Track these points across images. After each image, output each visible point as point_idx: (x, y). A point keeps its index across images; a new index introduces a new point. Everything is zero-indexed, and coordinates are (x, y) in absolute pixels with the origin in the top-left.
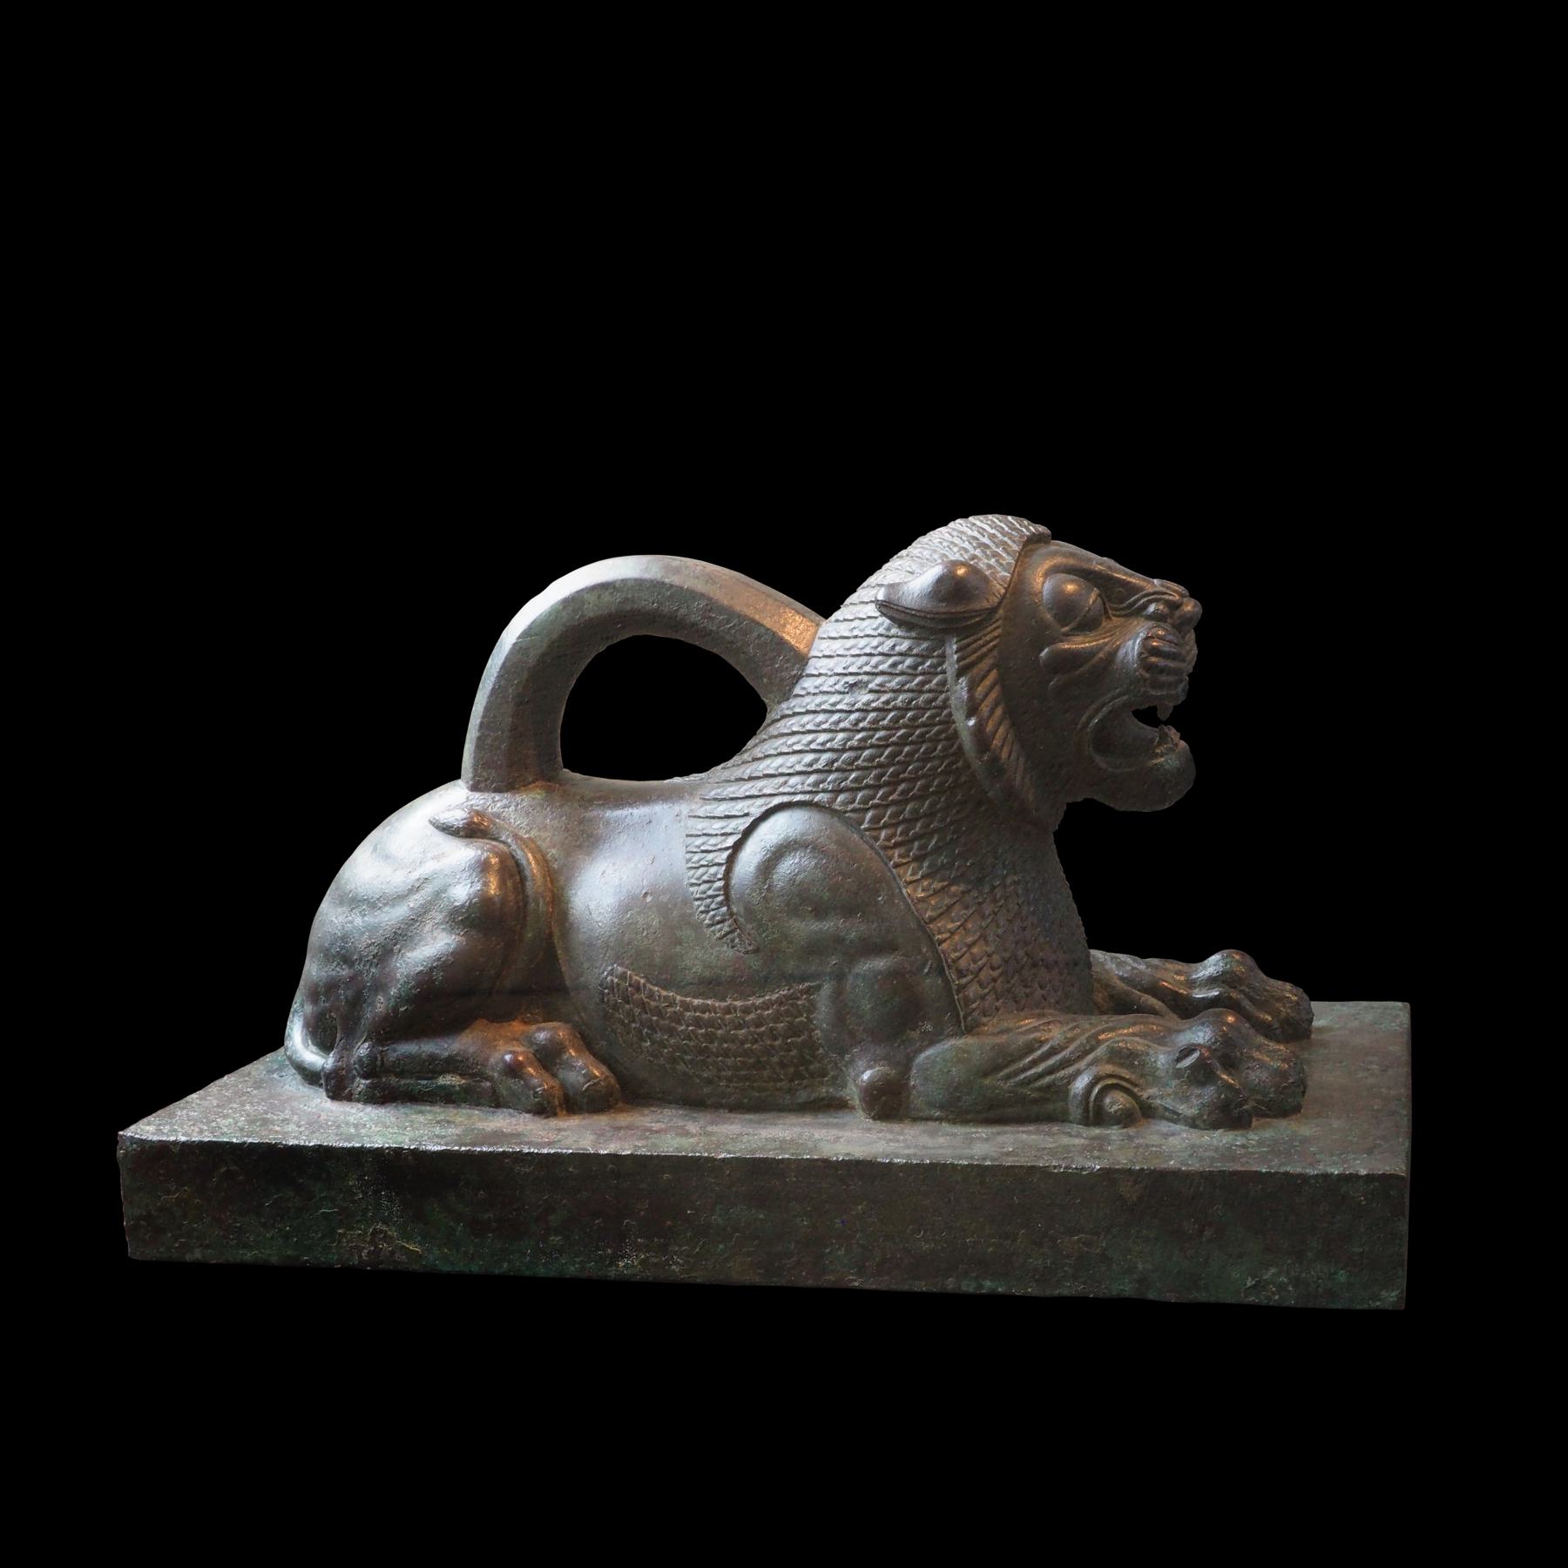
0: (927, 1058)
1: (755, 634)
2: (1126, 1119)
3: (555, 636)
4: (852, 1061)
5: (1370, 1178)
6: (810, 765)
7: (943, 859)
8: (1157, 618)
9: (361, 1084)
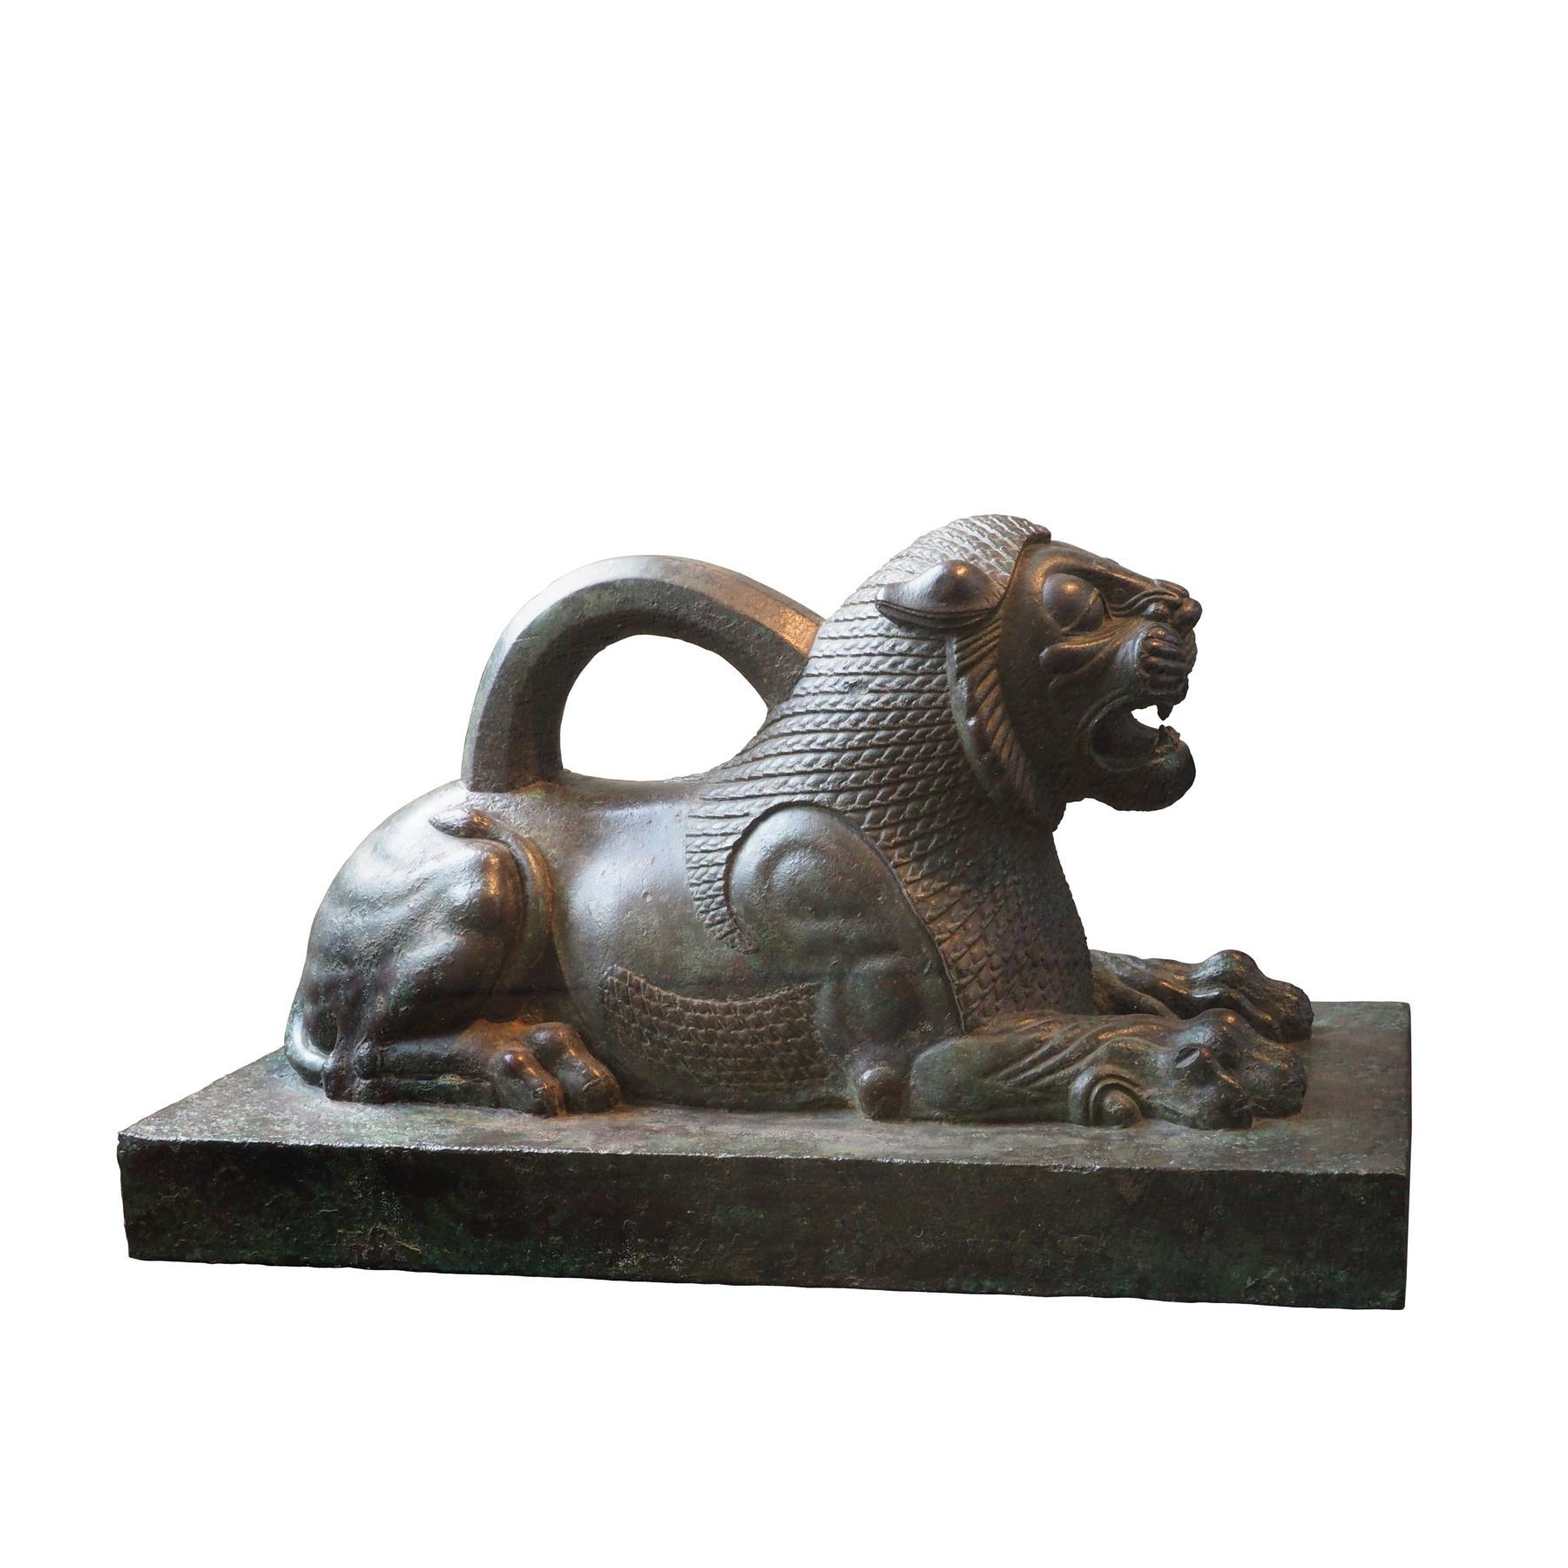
0: (927, 1058)
1: (755, 634)
2: (1126, 1119)
3: (555, 636)
4: (852, 1061)
5: (1370, 1178)
6: (810, 765)
7: (943, 859)
8: (1157, 618)
9: (361, 1084)
